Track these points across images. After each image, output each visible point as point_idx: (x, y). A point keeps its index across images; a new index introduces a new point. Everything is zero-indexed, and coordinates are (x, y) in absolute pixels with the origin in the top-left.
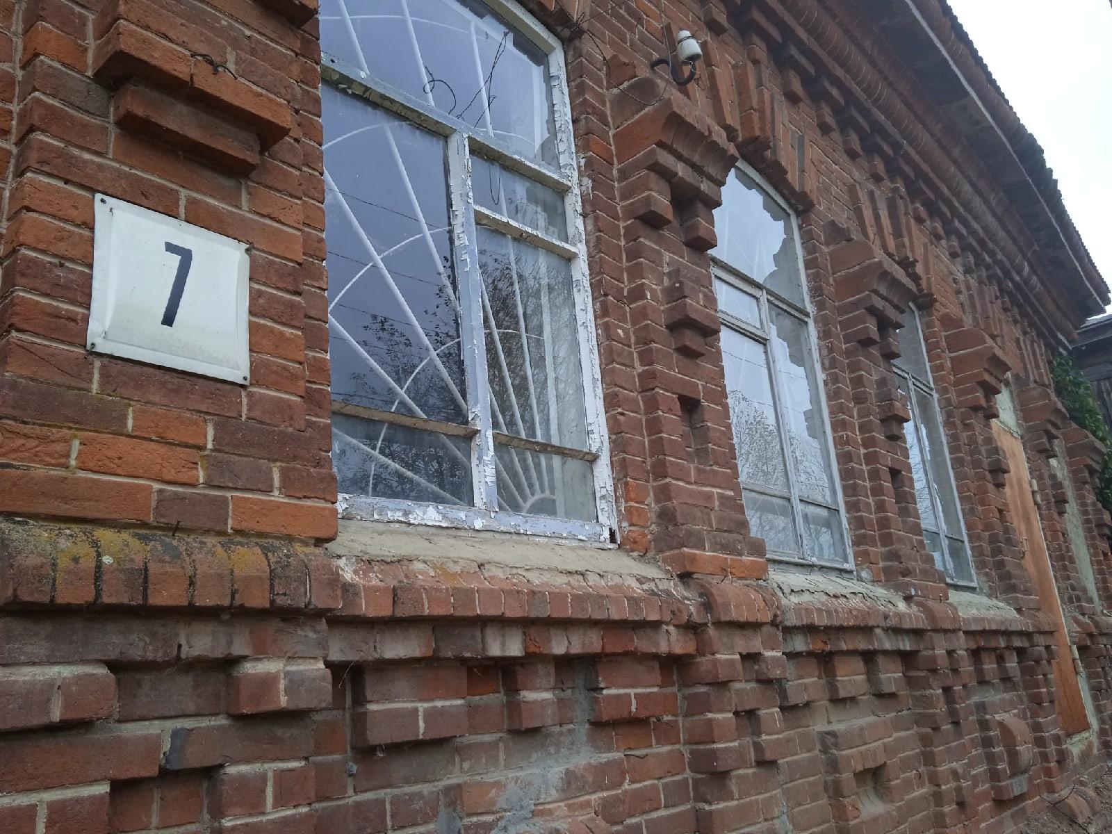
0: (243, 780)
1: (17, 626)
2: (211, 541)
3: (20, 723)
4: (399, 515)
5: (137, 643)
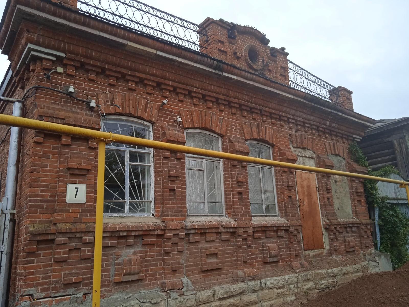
0: (83, 250)
1: (59, 234)
2: (79, 224)
3: (59, 243)
4: (111, 216)
5: (71, 236)
